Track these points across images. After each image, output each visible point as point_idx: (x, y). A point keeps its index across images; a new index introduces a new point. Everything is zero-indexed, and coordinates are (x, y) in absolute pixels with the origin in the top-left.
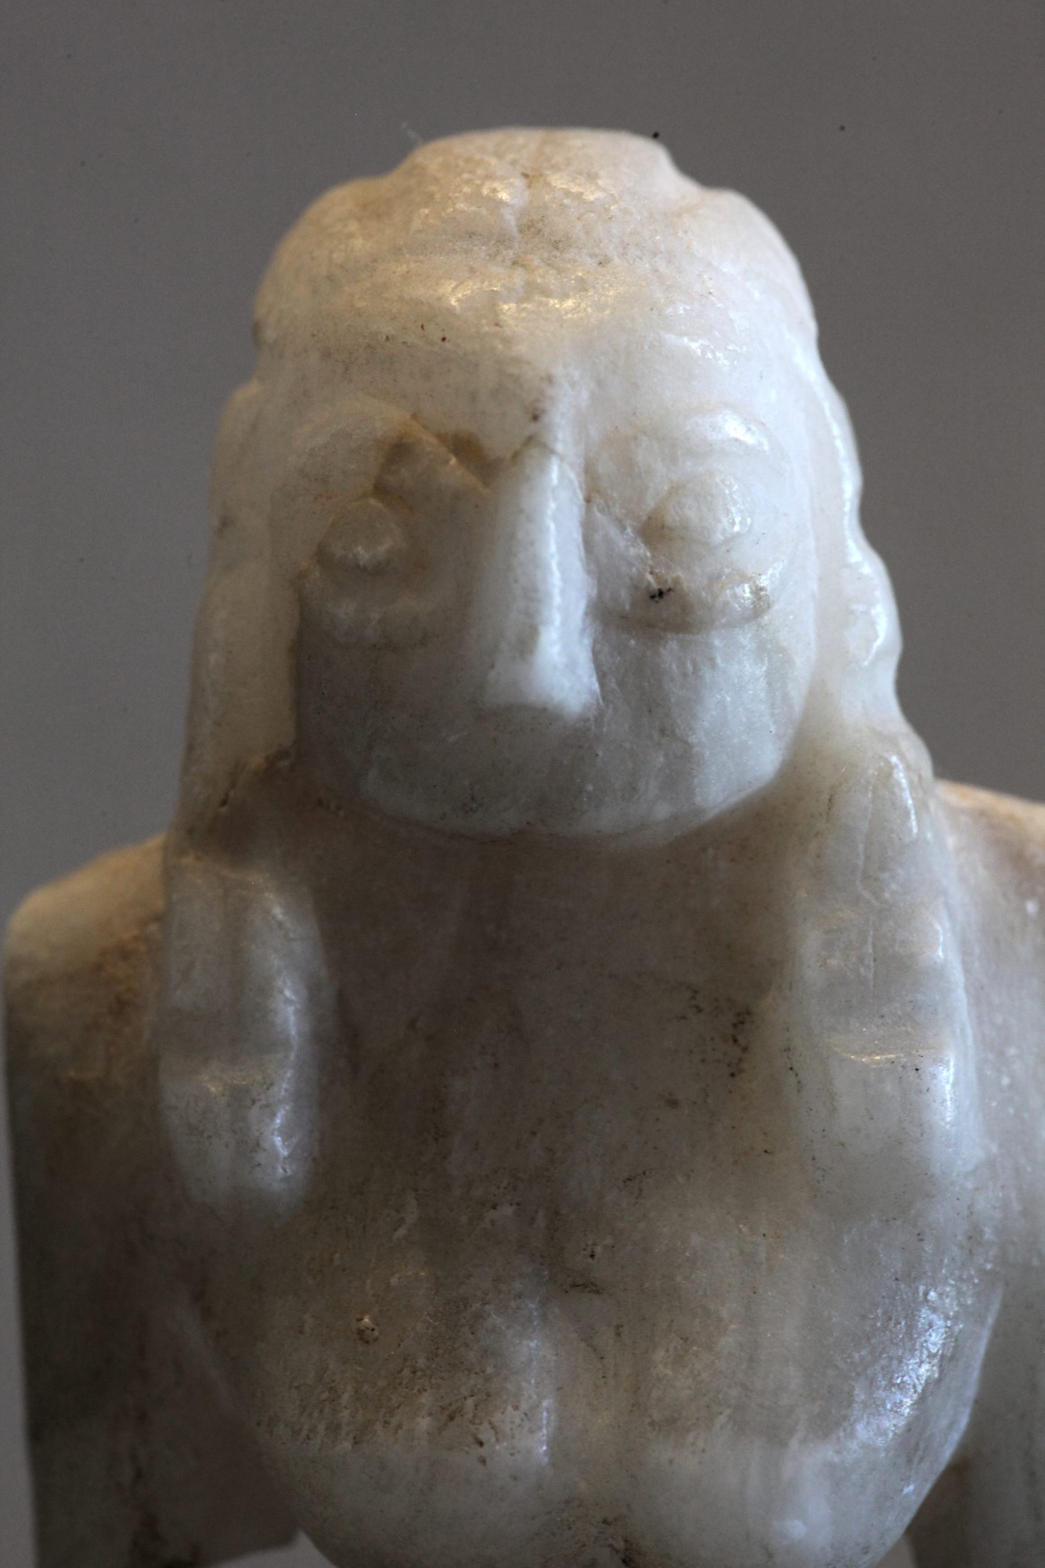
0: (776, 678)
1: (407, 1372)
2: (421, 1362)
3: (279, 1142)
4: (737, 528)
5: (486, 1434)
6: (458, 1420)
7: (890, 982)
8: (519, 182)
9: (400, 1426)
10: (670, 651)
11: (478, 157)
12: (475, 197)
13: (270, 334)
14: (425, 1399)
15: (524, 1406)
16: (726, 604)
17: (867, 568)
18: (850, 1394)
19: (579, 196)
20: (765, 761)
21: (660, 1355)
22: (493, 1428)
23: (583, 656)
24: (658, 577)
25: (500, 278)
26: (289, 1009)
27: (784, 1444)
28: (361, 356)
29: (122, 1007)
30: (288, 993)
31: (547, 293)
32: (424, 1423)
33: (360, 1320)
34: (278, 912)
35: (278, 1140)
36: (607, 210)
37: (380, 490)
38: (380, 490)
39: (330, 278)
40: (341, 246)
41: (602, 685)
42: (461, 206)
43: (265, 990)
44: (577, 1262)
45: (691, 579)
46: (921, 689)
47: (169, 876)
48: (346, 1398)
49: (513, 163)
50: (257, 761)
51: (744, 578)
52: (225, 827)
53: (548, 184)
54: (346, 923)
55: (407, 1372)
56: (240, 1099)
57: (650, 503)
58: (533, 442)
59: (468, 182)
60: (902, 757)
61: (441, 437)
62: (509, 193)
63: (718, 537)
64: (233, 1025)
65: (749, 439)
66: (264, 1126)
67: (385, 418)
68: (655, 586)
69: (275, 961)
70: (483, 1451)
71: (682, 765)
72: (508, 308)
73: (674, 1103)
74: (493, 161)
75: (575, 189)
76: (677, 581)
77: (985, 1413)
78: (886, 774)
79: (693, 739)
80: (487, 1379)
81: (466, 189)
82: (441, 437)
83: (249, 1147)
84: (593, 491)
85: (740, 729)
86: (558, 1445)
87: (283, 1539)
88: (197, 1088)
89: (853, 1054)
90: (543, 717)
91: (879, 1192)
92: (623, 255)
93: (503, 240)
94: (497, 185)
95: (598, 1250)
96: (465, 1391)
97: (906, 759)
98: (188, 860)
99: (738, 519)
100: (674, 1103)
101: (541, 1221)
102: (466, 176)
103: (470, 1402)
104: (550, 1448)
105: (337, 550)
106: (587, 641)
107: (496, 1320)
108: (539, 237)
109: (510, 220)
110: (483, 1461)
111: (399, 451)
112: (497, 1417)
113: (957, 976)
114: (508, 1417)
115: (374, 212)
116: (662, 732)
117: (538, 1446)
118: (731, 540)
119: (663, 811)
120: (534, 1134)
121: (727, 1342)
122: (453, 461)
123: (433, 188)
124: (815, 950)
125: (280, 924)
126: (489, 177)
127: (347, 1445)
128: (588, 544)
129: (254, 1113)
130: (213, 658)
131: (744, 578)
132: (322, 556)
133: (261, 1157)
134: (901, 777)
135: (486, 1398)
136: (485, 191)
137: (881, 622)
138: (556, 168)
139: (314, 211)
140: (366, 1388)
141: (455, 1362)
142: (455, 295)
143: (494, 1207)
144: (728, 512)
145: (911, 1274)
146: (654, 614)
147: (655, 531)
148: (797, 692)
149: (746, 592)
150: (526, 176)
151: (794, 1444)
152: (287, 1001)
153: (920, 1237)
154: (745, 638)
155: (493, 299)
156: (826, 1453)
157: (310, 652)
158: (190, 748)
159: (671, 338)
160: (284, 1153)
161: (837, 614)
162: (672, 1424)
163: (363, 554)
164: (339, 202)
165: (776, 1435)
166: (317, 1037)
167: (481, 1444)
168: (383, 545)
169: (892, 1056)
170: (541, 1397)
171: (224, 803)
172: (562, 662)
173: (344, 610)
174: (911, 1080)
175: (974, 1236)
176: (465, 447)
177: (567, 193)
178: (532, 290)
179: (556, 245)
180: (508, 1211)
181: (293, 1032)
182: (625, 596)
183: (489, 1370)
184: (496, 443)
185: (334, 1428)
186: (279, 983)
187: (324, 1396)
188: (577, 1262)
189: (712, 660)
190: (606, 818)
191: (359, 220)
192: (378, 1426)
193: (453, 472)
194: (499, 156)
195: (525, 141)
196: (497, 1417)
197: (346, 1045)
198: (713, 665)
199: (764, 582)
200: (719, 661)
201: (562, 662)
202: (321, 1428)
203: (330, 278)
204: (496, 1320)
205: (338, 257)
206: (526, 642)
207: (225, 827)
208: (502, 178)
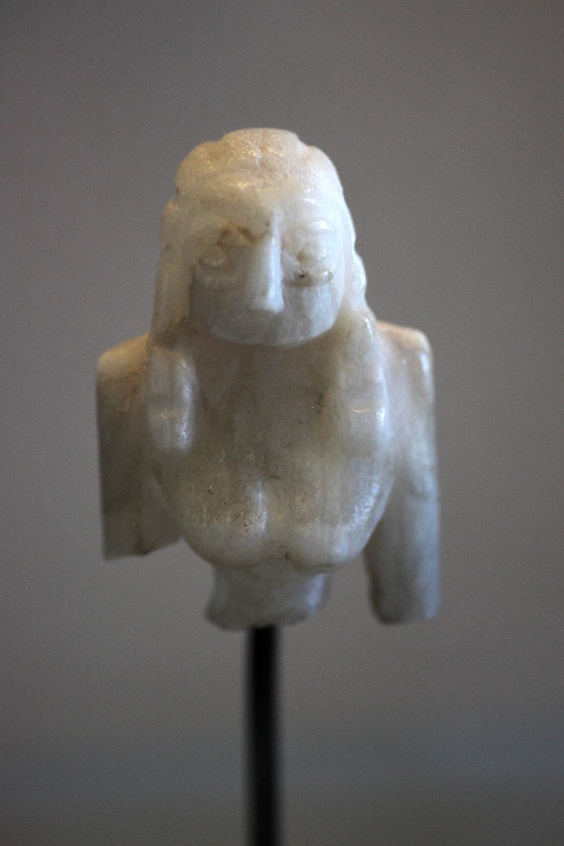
0: (333, 298)
1: (223, 503)
2: (228, 500)
3: (184, 433)
4: (324, 256)
5: (247, 523)
6: (239, 518)
7: (366, 387)
8: (259, 150)
9: (221, 520)
10: (305, 293)
11: (246, 141)
12: (246, 155)
13: (183, 193)
14: (229, 512)
15: (258, 514)
16: (321, 278)
17: (357, 261)
18: (354, 510)
19: (277, 155)
20: (330, 322)
21: (298, 499)
22: (249, 521)
23: (280, 294)
24: (302, 271)
25: (256, 182)
26: (187, 393)
27: (335, 526)
28: (212, 203)
29: (135, 390)
30: (187, 389)
31: (269, 186)
32: (228, 520)
33: (209, 487)
34: (184, 365)
35: (184, 433)
36: (286, 159)
37: (219, 244)
38: (219, 244)
39: (203, 178)
40: (202, 164)
41: (285, 303)
42: (242, 158)
43: (181, 389)
44: (273, 470)
45: (312, 271)
46: (372, 296)
47: (149, 352)
48: (205, 510)
49: (257, 143)
50: (178, 320)
51: (326, 270)
52: (167, 339)
53: (268, 151)
54: (202, 367)
55: (223, 503)
56: (173, 422)
57: (300, 249)
58: (267, 232)
59: (244, 150)
60: (369, 319)
61: (238, 229)
62: (256, 154)
63: (320, 258)
64: (170, 399)
65: (327, 228)
66: (180, 430)
67: (221, 223)
68: (301, 273)
69: (183, 380)
70: (246, 528)
71: (308, 325)
72: (258, 190)
73: (301, 422)
74: (250, 143)
75: (276, 153)
76: (307, 272)
77: (389, 510)
78: (365, 325)
79: (311, 318)
80: (247, 506)
81: (244, 152)
82: (238, 229)
83: (175, 435)
84: (284, 246)
85: (323, 315)
86: (267, 525)
87: (173, 538)
88: (159, 417)
89: (355, 410)
90: (268, 313)
91: (360, 449)
92: (291, 173)
93: (255, 169)
94: (253, 151)
95: (279, 467)
96: (241, 510)
97: (368, 319)
98: (156, 348)
99: (325, 253)
100: (301, 422)
101: (262, 457)
102: (243, 148)
103: (242, 513)
104: (266, 526)
105: (206, 261)
106: (281, 290)
107: (249, 488)
108: (266, 168)
109: (257, 163)
110: (246, 531)
111: (225, 233)
112: (250, 518)
113: (384, 384)
114: (254, 518)
115: (214, 156)
116: (302, 316)
117: (262, 526)
118: (324, 258)
119: (301, 339)
120: (260, 431)
121: (318, 495)
122: (242, 236)
123: (233, 152)
124: (343, 378)
125: (185, 369)
126: (250, 148)
127: (205, 525)
128: (282, 262)
129: (178, 425)
130: (164, 289)
131: (326, 270)
132: (200, 261)
133: (179, 439)
134: (369, 326)
135: (247, 512)
136: (249, 153)
137: (362, 279)
138: (269, 145)
139: (194, 153)
140: (211, 508)
141: (238, 500)
142: (242, 186)
143: (248, 453)
144: (322, 251)
145: (370, 473)
146: (300, 281)
147: (301, 257)
148: (339, 302)
149: (326, 273)
150: (261, 148)
151: (338, 526)
152: (187, 391)
153: (372, 462)
154: (326, 287)
155: (254, 188)
156: (348, 528)
157: (194, 288)
158: (157, 314)
159: (306, 200)
160: (186, 437)
161: (350, 278)
162: (302, 520)
163: (214, 263)
164: (202, 151)
165: (333, 523)
166: (195, 402)
167: (246, 526)
168: (219, 261)
169: (367, 410)
170: (263, 511)
171: (167, 332)
172: (274, 298)
173: (208, 279)
174: (373, 417)
175: (388, 462)
176: (246, 232)
177: (274, 154)
178: (266, 185)
179: (271, 170)
180: (252, 455)
181: (188, 401)
182: (292, 276)
183: (248, 503)
184: (255, 232)
185: (201, 520)
186: (184, 386)
187: (198, 510)
188: (273, 470)
189: (317, 294)
190: (285, 341)
191: (211, 160)
192: (215, 520)
193: (242, 240)
194: (252, 141)
195: (258, 133)
196: (250, 518)
197: (202, 402)
198: (317, 296)
199: (331, 270)
200: (319, 294)
201: (274, 298)
202: (198, 519)
203: (203, 178)
204: (249, 488)
205: (205, 172)
206: (264, 293)
207: (167, 339)
208: (254, 149)
